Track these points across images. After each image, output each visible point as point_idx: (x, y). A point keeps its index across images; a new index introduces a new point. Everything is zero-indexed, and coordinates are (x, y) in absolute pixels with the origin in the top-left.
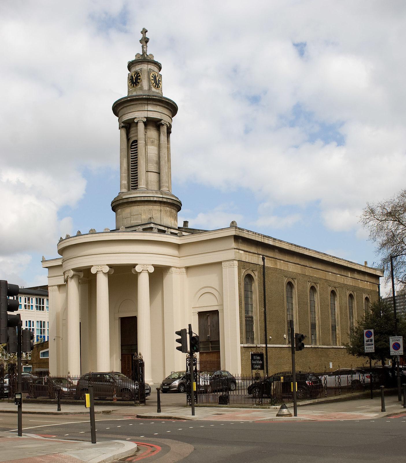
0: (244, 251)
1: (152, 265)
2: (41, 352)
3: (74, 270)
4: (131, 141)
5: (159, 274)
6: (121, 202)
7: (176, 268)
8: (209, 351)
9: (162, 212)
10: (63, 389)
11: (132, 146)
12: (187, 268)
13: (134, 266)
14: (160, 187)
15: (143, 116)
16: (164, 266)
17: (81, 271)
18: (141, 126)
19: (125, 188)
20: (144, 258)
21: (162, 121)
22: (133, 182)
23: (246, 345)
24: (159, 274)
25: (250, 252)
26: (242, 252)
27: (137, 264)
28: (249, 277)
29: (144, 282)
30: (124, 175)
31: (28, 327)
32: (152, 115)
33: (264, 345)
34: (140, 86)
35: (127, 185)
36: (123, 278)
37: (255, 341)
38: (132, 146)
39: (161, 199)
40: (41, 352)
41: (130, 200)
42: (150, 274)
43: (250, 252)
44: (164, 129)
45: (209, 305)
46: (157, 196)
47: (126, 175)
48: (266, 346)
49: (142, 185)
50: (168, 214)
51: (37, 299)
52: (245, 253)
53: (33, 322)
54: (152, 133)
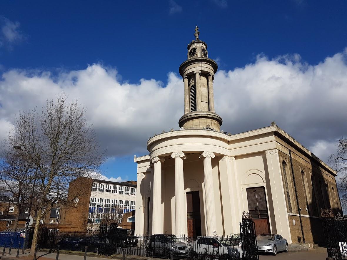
0: (280, 144)
1: (214, 153)
2: (128, 218)
3: (159, 157)
4: (191, 86)
5: (216, 160)
6: (186, 118)
7: (228, 156)
8: (258, 218)
9: (212, 124)
10: (217, 249)
11: (191, 89)
12: (236, 157)
13: (202, 152)
14: (209, 111)
15: (199, 70)
16: (220, 155)
17: (163, 158)
18: (198, 76)
19: (188, 112)
20: (208, 148)
21: (210, 73)
22: (194, 107)
23: (290, 214)
24: (216, 160)
25: (283, 145)
26: (279, 144)
27: (204, 152)
28: (284, 162)
29: (208, 163)
30: (187, 104)
31: (120, 204)
32: (203, 69)
33: (299, 215)
34: (196, 55)
35: (189, 110)
36: (194, 161)
37: (293, 211)
38: (191, 89)
39: (212, 116)
40: (128, 218)
41: (192, 116)
42: (212, 158)
43: (283, 145)
44: (210, 78)
45: (260, 182)
46: (209, 114)
47: (188, 104)
48: (300, 215)
49: (199, 108)
50: (216, 125)
51: (126, 188)
52: (281, 145)
53: (123, 201)
54: (204, 79)
